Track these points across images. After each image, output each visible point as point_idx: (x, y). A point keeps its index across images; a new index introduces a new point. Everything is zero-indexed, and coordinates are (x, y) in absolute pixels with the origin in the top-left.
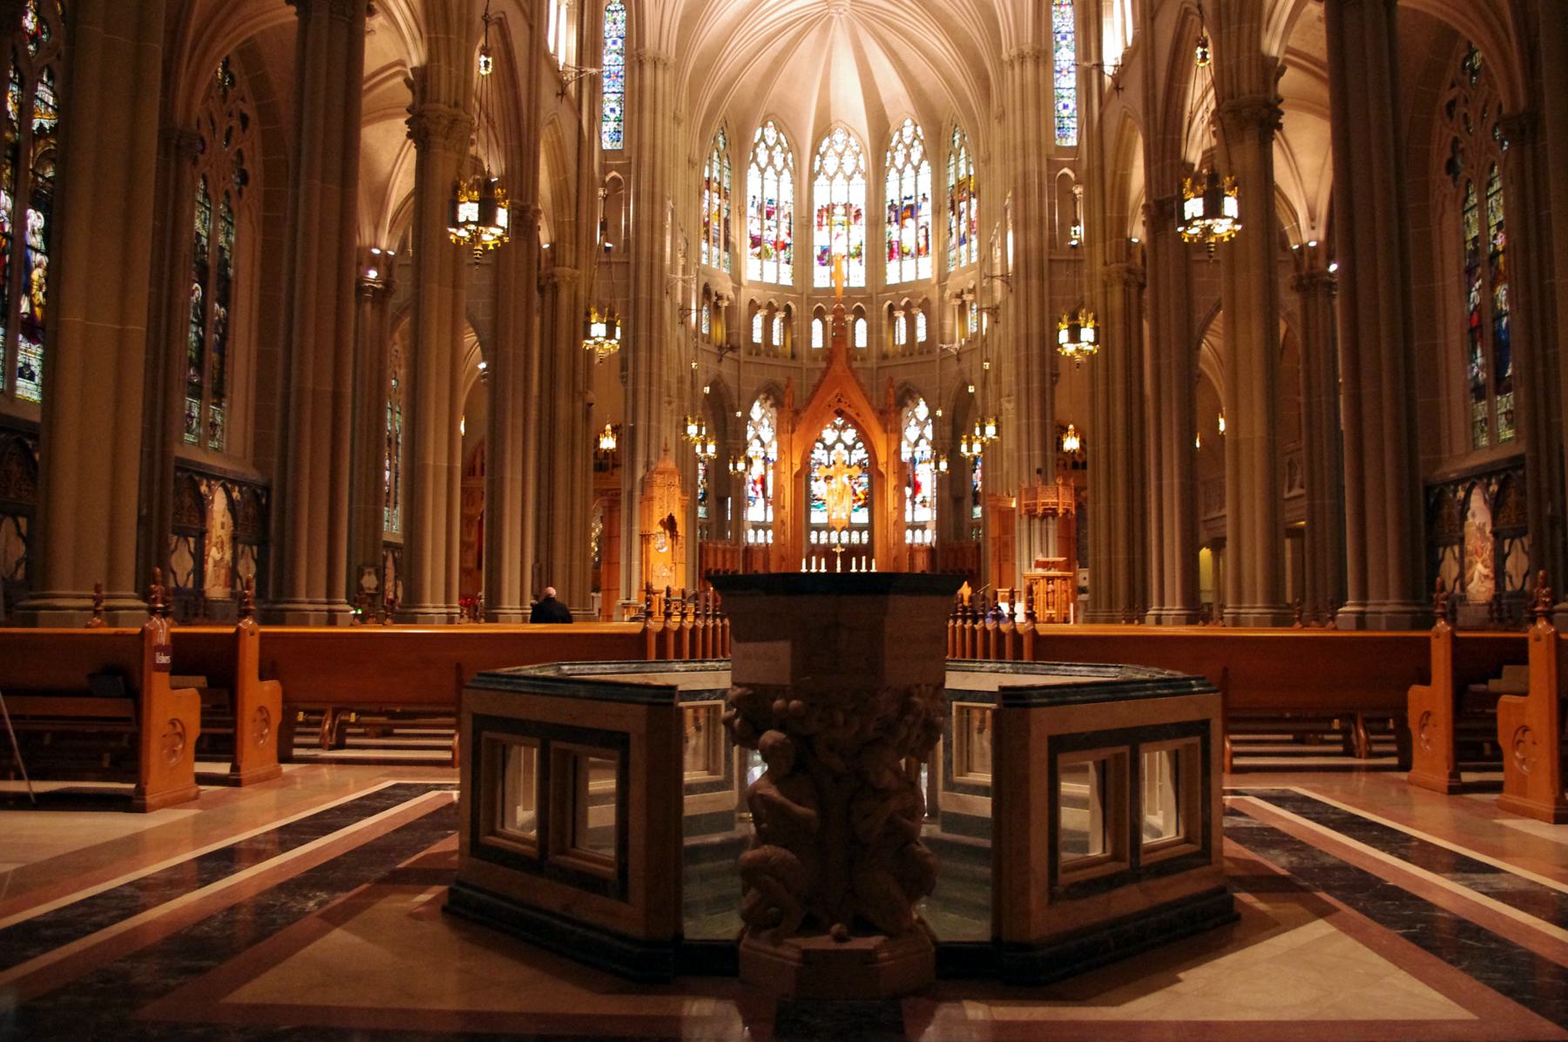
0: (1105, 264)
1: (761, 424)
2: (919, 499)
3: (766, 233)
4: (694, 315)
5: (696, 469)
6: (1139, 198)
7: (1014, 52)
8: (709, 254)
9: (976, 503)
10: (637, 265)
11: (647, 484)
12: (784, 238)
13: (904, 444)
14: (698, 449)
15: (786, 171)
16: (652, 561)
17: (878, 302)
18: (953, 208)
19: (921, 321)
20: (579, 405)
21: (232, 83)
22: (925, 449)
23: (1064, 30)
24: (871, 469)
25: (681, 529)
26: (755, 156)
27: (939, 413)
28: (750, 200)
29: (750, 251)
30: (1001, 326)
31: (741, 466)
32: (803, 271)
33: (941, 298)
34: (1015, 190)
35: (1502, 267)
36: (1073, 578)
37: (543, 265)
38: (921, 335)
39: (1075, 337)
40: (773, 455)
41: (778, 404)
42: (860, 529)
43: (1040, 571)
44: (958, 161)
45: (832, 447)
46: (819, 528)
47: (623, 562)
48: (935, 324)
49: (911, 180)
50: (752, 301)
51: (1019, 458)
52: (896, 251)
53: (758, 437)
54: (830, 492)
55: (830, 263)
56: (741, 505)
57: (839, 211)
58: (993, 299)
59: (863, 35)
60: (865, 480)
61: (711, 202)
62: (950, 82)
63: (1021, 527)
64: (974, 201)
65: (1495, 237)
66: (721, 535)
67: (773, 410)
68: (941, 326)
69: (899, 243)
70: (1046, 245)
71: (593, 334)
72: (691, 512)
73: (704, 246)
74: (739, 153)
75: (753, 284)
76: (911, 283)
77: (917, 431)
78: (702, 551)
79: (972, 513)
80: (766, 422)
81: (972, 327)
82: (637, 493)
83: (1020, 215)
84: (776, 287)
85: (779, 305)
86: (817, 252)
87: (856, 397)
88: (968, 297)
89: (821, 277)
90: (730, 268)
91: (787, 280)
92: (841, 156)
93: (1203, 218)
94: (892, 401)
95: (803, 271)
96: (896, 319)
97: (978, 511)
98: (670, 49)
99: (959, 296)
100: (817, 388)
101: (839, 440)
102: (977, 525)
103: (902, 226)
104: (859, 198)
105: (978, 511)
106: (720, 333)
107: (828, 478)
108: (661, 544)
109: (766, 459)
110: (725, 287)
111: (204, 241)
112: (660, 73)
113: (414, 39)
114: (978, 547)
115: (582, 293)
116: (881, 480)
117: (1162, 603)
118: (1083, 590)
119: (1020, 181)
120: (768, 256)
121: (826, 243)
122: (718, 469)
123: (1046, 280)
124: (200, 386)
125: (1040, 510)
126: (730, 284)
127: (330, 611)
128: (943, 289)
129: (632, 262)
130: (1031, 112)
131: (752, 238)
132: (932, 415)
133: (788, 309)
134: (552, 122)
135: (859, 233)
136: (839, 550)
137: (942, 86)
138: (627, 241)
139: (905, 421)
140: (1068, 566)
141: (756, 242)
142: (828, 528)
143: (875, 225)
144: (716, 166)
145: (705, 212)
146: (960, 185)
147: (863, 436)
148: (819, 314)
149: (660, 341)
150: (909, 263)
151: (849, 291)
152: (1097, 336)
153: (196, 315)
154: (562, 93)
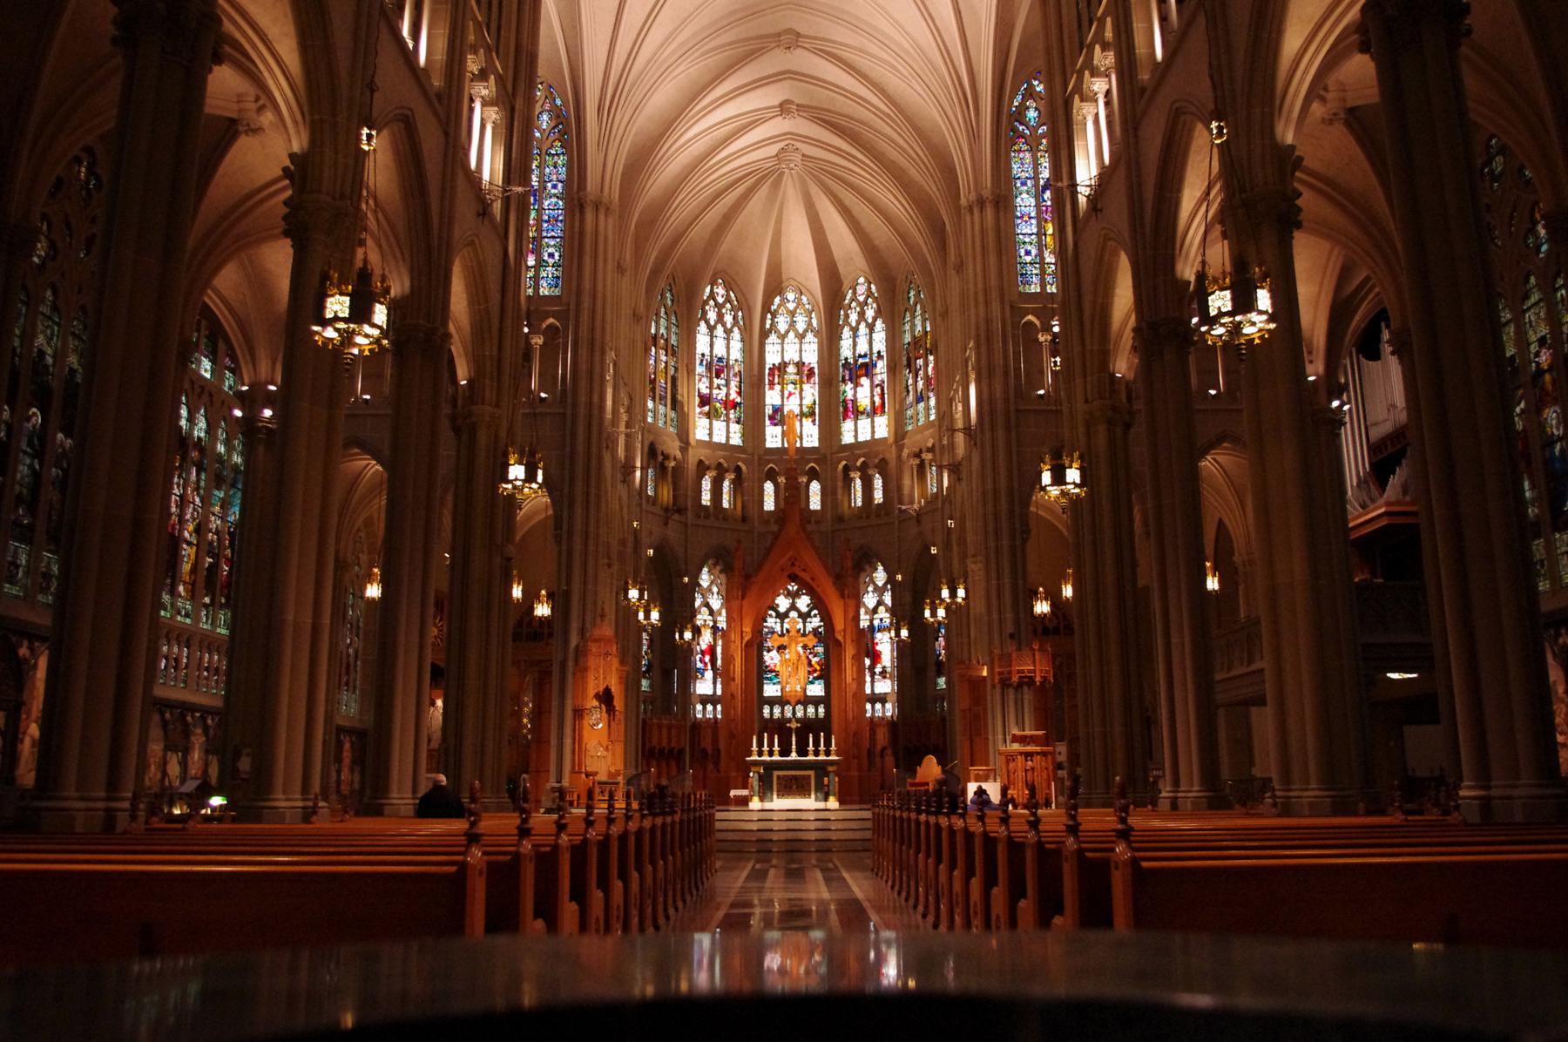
0: (1086, 401)
1: (711, 598)
2: (878, 669)
3: (715, 392)
4: (638, 474)
5: (640, 639)
6: (1128, 317)
7: (973, 197)
8: (655, 412)
9: (939, 674)
10: (574, 416)
11: (581, 653)
12: (733, 395)
13: (862, 611)
14: (641, 616)
15: (736, 330)
16: (585, 739)
17: (832, 461)
18: (909, 365)
19: (878, 483)
20: (497, 560)
21: (99, 186)
22: (883, 615)
23: (1024, 175)
24: (827, 637)
25: (618, 703)
26: (705, 313)
27: (899, 577)
28: (698, 357)
29: (698, 410)
30: (964, 483)
31: (688, 635)
32: (754, 431)
33: (899, 457)
34: (978, 337)
35: (1549, 387)
36: (1053, 754)
37: (460, 402)
38: (878, 496)
39: (1059, 479)
40: (722, 624)
41: (728, 570)
42: (816, 701)
43: (1016, 746)
44: (913, 317)
45: (786, 615)
46: (772, 702)
47: (554, 741)
48: (893, 486)
49: (866, 339)
50: (701, 462)
51: (990, 624)
52: (856, 412)
53: (707, 605)
54: (784, 662)
55: (782, 423)
56: (690, 675)
57: (791, 369)
58: (954, 455)
59: (815, 190)
60: (820, 650)
61: (658, 359)
62: (903, 236)
63: (994, 698)
64: (931, 358)
65: (1537, 354)
66: (667, 710)
67: (723, 577)
68: (900, 488)
69: (854, 401)
70: (1012, 396)
71: (511, 477)
72: (631, 684)
73: (650, 404)
74: (688, 314)
75: (700, 442)
76: (866, 442)
77: (875, 601)
78: (645, 728)
79: (936, 684)
80: (715, 589)
81: (932, 488)
82: (571, 664)
83: (984, 362)
84: (726, 446)
85: (724, 463)
86: (769, 411)
87: (811, 560)
88: (927, 456)
89: (773, 437)
90: (677, 427)
91: (736, 440)
92: (793, 314)
93: (1231, 314)
94: (850, 564)
95: (754, 431)
96: (852, 480)
97: (942, 681)
98: (614, 193)
99: (918, 455)
100: (769, 550)
101: (793, 607)
102: (941, 696)
103: (857, 385)
104: (811, 357)
105: (942, 681)
106: (666, 494)
107: (781, 648)
108: (596, 724)
109: (715, 629)
110: (673, 447)
111: (50, 360)
112: (602, 217)
113: (295, 122)
114: (944, 719)
115: (503, 434)
116: (839, 649)
117: (1176, 783)
118: (1059, 766)
119: (983, 327)
120: (718, 417)
121: (778, 402)
122: (663, 635)
123: (1015, 432)
124: (31, 528)
125: (1015, 679)
126: (677, 444)
127: (107, 810)
128: (900, 448)
129: (569, 412)
130: (992, 259)
131: (700, 396)
132: (890, 580)
133: (738, 470)
134: (472, 243)
135: (811, 392)
136: (794, 725)
137: (897, 243)
138: (564, 391)
139: (862, 587)
140: (1046, 741)
141: (705, 400)
142: (781, 701)
143: (829, 385)
144: (663, 322)
145: (651, 369)
146: (917, 342)
147: (818, 603)
148: (771, 476)
149: (598, 497)
150: (864, 423)
151: (803, 450)
152: (1082, 476)
153: (30, 444)
154: (484, 211)
